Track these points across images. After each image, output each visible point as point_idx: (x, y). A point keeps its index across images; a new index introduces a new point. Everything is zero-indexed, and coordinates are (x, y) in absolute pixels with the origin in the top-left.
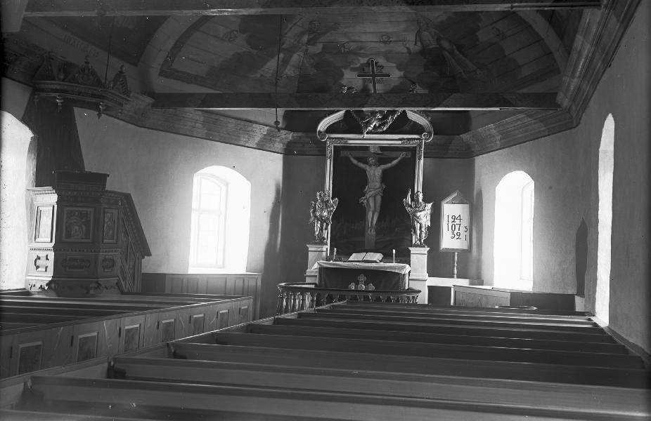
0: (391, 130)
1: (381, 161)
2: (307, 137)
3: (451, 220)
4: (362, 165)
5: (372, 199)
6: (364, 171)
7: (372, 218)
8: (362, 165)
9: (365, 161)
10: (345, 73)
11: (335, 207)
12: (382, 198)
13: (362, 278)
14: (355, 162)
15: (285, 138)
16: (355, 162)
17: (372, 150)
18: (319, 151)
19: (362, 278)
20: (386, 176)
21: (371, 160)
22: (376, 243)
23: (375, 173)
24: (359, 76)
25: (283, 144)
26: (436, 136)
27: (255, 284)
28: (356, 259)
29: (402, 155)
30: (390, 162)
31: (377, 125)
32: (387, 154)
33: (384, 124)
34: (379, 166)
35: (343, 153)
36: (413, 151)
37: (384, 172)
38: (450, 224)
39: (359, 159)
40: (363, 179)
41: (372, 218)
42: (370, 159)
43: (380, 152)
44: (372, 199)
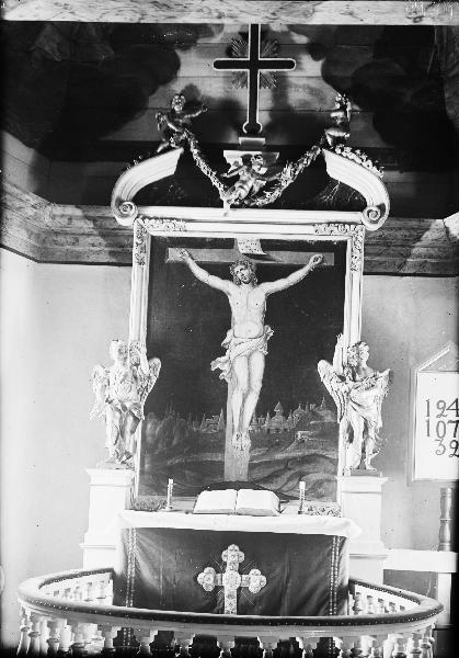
0: (289, 201)
1: (264, 273)
2: (87, 218)
3: (435, 411)
4: (215, 282)
5: (244, 359)
6: (222, 297)
7: (242, 403)
8: (215, 282)
9: (223, 271)
10: (182, 60)
11: (154, 380)
12: (267, 359)
13: (232, 555)
14: (201, 274)
15: (36, 218)
16: (201, 274)
17: (242, 249)
18: (111, 253)
19: (232, 555)
20: (275, 310)
21: (242, 272)
22: (252, 467)
23: (247, 304)
24: (218, 65)
25: (30, 233)
26: (396, 223)
27: (7, 244)
28: (215, 511)
29: (312, 261)
30: (285, 276)
31: (256, 189)
32: (283, 258)
33: (269, 187)
34: (259, 283)
35: (175, 255)
36: (339, 249)
37: (272, 299)
38: (434, 421)
39: (211, 268)
40: (219, 314)
41: (242, 403)
42: (237, 269)
43: (261, 252)
44: (244, 359)
